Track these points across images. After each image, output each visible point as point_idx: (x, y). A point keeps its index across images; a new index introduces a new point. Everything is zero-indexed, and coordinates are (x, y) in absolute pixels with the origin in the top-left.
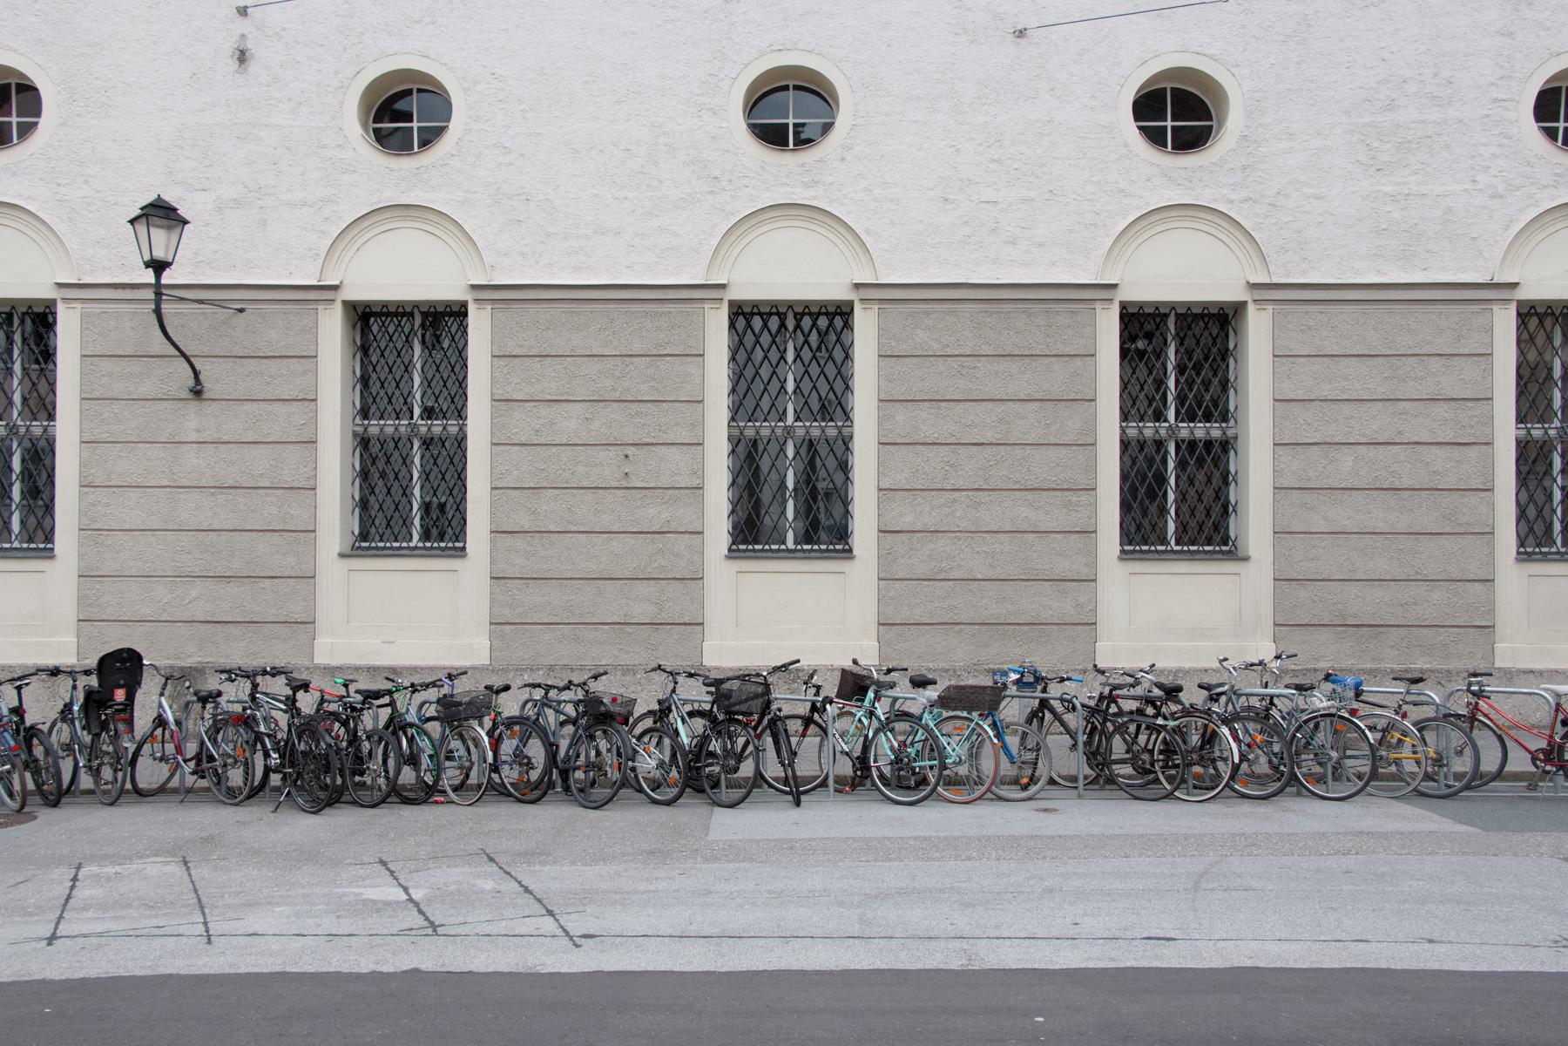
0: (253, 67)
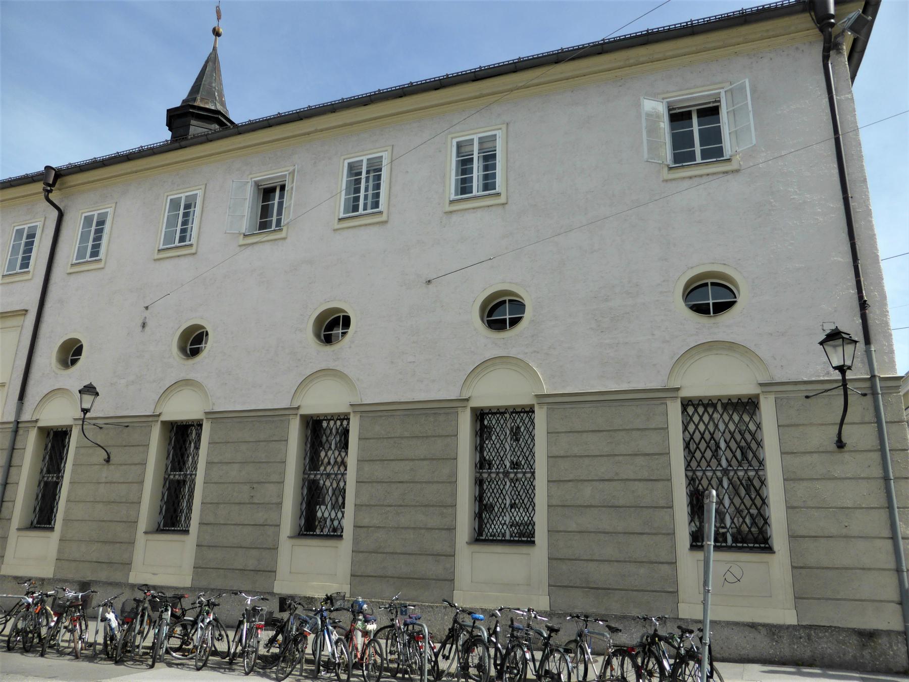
0: (147, 329)
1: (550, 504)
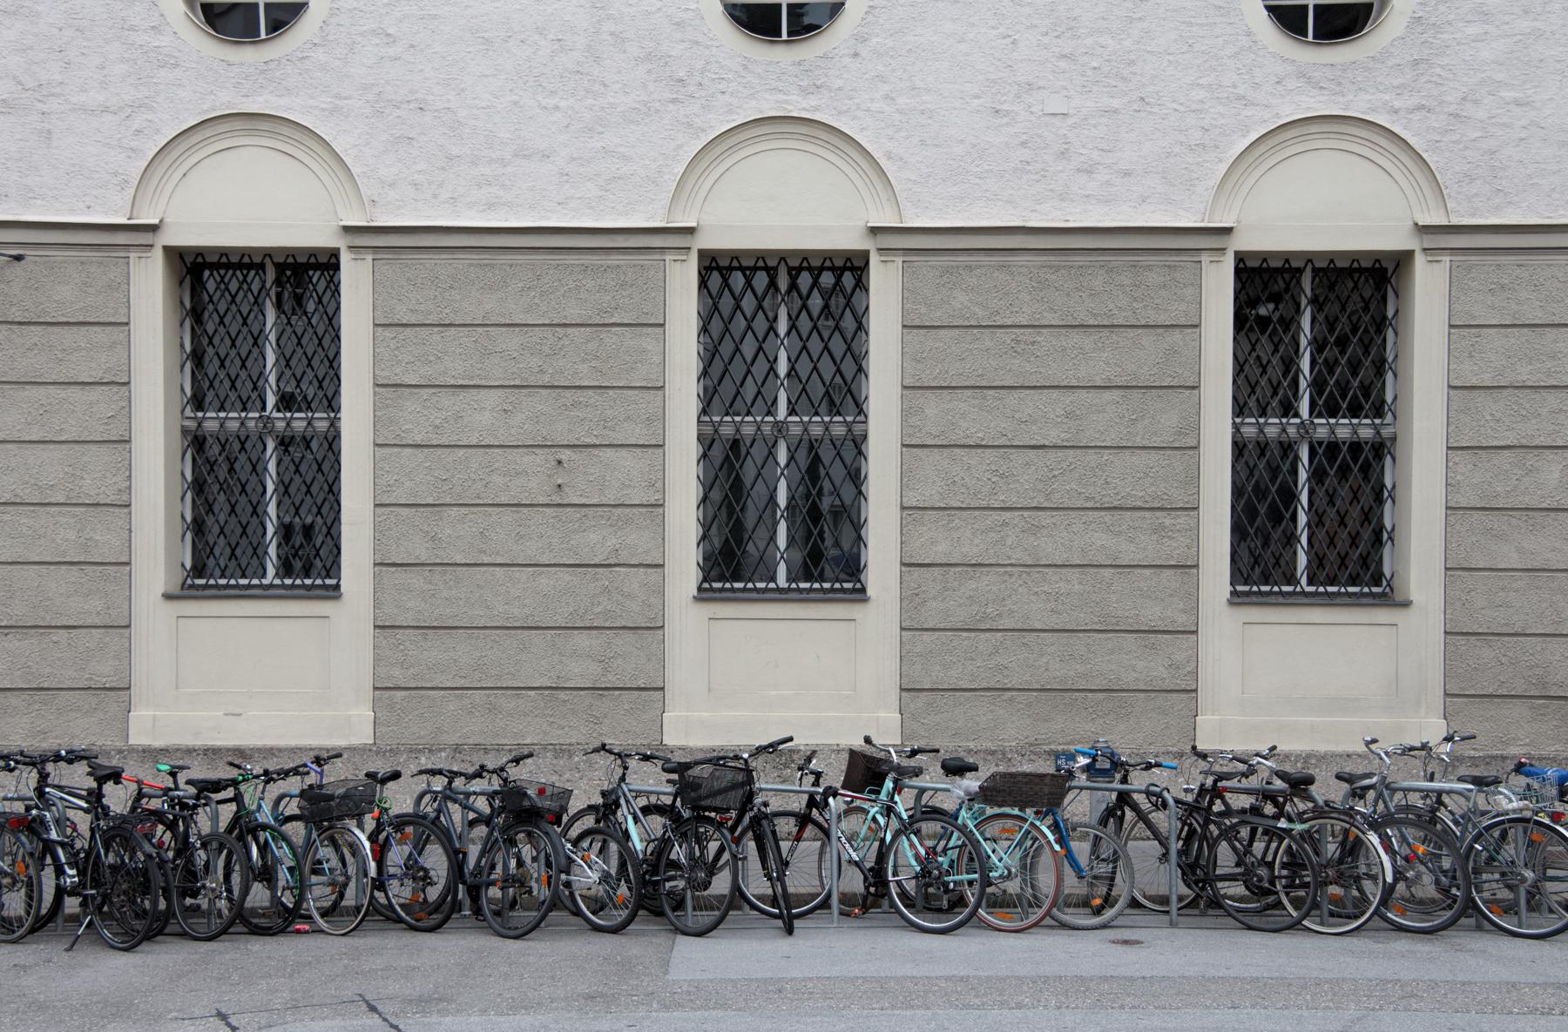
1: (1453, 505)
